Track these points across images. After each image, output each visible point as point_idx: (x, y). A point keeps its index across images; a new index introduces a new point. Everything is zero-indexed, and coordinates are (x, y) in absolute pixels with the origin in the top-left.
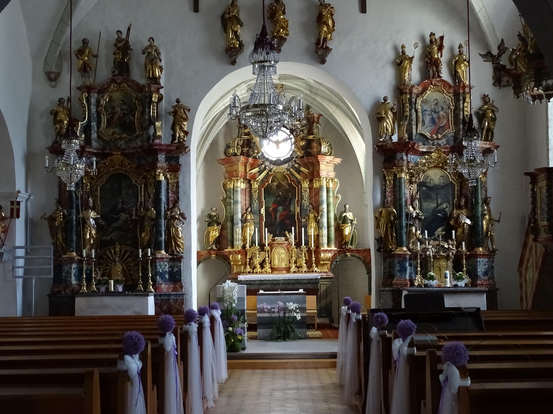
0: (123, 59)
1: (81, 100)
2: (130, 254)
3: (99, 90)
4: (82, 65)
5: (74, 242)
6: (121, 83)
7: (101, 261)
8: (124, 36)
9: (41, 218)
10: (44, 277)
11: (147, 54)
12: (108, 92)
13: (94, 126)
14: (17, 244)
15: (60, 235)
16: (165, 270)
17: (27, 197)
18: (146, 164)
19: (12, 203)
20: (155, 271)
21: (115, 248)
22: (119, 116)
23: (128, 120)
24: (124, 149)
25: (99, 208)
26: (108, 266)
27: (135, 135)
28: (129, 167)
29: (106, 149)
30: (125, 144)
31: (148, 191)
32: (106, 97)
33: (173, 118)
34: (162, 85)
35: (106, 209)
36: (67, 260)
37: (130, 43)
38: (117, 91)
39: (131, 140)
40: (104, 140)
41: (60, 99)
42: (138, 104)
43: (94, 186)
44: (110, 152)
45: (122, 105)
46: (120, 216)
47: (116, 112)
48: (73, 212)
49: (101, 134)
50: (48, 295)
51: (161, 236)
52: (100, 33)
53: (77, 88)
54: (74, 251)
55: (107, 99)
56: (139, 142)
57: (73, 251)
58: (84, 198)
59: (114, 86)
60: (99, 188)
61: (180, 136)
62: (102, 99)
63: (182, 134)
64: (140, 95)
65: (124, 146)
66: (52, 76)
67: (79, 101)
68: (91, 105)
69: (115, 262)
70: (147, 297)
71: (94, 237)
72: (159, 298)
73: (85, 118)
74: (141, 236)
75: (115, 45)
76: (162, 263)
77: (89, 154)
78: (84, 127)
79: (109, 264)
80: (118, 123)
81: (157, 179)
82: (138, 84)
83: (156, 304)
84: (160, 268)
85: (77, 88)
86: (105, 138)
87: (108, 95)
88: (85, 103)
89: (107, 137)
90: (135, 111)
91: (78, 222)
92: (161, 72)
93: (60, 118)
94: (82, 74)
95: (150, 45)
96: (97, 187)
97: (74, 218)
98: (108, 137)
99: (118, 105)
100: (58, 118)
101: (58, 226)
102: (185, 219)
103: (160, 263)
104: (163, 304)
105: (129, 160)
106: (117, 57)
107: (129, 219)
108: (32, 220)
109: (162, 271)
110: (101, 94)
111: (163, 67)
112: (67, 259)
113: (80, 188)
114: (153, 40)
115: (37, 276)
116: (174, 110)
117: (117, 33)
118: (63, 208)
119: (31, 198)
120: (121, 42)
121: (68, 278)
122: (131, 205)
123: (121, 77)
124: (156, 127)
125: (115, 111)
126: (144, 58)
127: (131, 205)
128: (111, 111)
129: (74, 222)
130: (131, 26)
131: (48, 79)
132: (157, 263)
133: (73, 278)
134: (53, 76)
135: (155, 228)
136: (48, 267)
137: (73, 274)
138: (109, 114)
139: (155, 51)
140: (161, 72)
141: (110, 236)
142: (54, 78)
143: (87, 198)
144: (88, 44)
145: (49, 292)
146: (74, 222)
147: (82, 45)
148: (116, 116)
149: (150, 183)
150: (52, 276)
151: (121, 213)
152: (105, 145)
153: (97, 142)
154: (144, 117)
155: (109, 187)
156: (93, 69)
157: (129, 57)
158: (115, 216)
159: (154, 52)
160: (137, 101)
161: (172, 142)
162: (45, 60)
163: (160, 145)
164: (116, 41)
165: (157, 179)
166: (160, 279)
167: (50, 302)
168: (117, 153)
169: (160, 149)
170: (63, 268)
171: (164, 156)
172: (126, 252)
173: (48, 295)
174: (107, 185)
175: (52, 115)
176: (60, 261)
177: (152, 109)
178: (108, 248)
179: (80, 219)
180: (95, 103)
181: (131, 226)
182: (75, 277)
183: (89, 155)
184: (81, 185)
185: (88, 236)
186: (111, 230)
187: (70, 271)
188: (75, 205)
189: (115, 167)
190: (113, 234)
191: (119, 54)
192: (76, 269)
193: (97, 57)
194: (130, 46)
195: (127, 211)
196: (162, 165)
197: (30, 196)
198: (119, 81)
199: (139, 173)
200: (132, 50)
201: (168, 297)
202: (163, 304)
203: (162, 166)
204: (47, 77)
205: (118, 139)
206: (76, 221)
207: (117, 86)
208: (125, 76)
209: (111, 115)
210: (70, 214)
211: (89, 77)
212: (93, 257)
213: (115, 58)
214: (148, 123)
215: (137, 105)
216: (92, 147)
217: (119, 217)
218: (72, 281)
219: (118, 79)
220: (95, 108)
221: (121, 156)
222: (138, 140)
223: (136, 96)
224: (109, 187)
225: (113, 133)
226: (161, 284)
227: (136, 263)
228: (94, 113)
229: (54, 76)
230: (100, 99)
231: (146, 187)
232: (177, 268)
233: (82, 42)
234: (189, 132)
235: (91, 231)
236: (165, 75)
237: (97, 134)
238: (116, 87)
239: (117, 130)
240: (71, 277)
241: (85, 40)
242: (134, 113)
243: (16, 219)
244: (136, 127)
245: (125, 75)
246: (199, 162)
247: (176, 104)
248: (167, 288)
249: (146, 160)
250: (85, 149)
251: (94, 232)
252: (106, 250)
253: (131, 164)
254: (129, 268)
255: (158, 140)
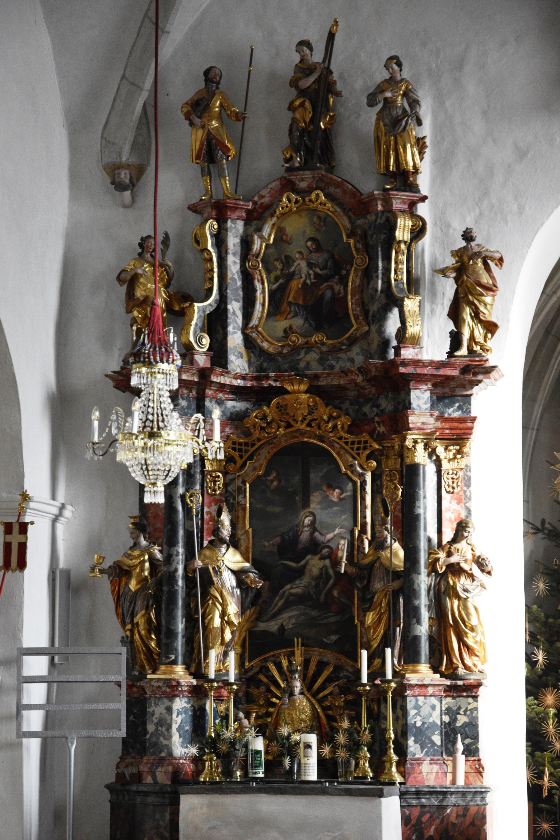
0: (314, 120)
1: (198, 240)
2: (332, 672)
3: (248, 212)
4: (202, 144)
5: (180, 636)
6: (310, 191)
7: (254, 691)
8: (317, 57)
9: (93, 569)
10: (101, 734)
11: (380, 106)
12: (272, 215)
13: (234, 313)
14: (28, 642)
15: (143, 615)
16: (431, 720)
17: (55, 511)
18: (376, 419)
19: (8, 528)
20: (401, 722)
21: (293, 654)
22: (305, 281)
23: (329, 294)
24: (316, 377)
25: (246, 541)
26: (274, 705)
27: (347, 335)
28: (330, 425)
29: (268, 378)
30: (321, 361)
31: (381, 493)
32: (268, 231)
33: (455, 286)
34: (424, 190)
35: (266, 544)
36: (159, 687)
37: (335, 76)
38: (299, 211)
39: (335, 350)
40: (262, 351)
41: (142, 239)
42: (357, 250)
43: (234, 479)
44: (278, 384)
45: (311, 252)
46: (307, 563)
47: (294, 271)
48: (178, 552)
49: (254, 335)
50: (108, 787)
51: (419, 622)
52: (252, 50)
53: (189, 208)
54: (180, 662)
55: (270, 235)
56: (357, 354)
57: (174, 662)
58: (208, 513)
59: (289, 200)
60: (248, 485)
61: (472, 338)
62: (256, 237)
63: (479, 333)
64: (360, 222)
65: (316, 369)
66: (123, 176)
67: (196, 245)
68: (227, 253)
69: (292, 694)
70: (377, 800)
71: (233, 623)
72: (414, 802)
73: (210, 290)
74: (362, 623)
75: (294, 83)
76: (421, 699)
77: (221, 391)
78: (208, 314)
79: (274, 700)
80: (301, 302)
81: (408, 461)
82: (356, 193)
83: (406, 820)
84: (418, 714)
85: (189, 208)
86: (265, 345)
87: (274, 225)
88: (210, 248)
89: (272, 344)
90: (348, 267)
91: (189, 580)
92: (421, 153)
93: (143, 293)
94: (202, 170)
95: (391, 78)
96: (244, 483)
97: (180, 571)
98: (274, 342)
99: (300, 253)
100: (139, 293)
101: (137, 592)
102: (489, 573)
103: (417, 701)
104: (425, 818)
105: (329, 408)
106: (298, 116)
107: (331, 572)
108: (67, 573)
109: (423, 723)
110: (254, 222)
111: (428, 141)
112: (161, 684)
113: (198, 487)
114: (399, 64)
115: (84, 733)
116: (457, 262)
117: (301, 47)
118: (153, 541)
119: (68, 513)
120: (310, 74)
121: (162, 739)
122: (336, 532)
123: (307, 172)
124: (407, 313)
125: (292, 269)
126: (374, 118)
127: (336, 532)
128: (282, 270)
129: (180, 582)
130: (337, 26)
131: (112, 183)
132: (408, 699)
133: (176, 739)
134: (124, 176)
135: (401, 600)
136: (112, 706)
137: (175, 727)
138: (277, 279)
139: (405, 95)
140: (421, 153)
141: (280, 621)
142: (127, 181)
143: (214, 514)
144: (218, 83)
145: (112, 779)
146: (180, 582)
147: (204, 86)
148: (296, 284)
149: (390, 471)
150: (123, 733)
151: (309, 557)
152: (265, 365)
153: (242, 358)
154: (371, 286)
155: (275, 483)
156: (232, 152)
157: (331, 117)
158: (293, 564)
159: (402, 99)
160: (352, 241)
161: (450, 354)
162: (102, 134)
163: (416, 363)
164: (295, 73)
165: (408, 461)
166: (418, 746)
167: (114, 807)
168: (296, 387)
169: (417, 374)
170: (150, 710)
171: (428, 394)
172: (322, 665)
173: (108, 787)
174: (271, 477)
175: (121, 285)
176: (143, 689)
177: (396, 263)
178: (271, 653)
179: (194, 571)
180: (238, 249)
181: (335, 593)
182: (180, 736)
183: (220, 395)
184: (198, 477)
185: (217, 622)
186: (280, 604)
187: (168, 718)
188: (181, 532)
189: (292, 426)
190: (285, 615)
191: (305, 109)
192: (186, 712)
193: (244, 118)
194: (335, 82)
195: (325, 551)
196: (423, 420)
197: (62, 507)
198: (303, 185)
199: (359, 443)
200: (338, 94)
201: (441, 801)
202: (425, 818)
203: (423, 424)
204: (109, 180)
205: (300, 347)
206: (186, 577)
207: (299, 198)
208: (319, 171)
209: (281, 281)
210: (169, 558)
211: (221, 175)
212: (232, 680)
213: (294, 120)
214: (384, 300)
215: (354, 253)
216: (228, 372)
217: (304, 566)
218: (174, 748)
219: (303, 180)
220: (238, 261)
221: (308, 395)
222: (356, 349)
223: (349, 226)
224: (275, 483)
225: (288, 332)
226: (419, 762)
227: (350, 697)
228: (236, 276)
229: (128, 176)
230: (252, 236)
231: (378, 482)
232: (465, 714)
233: (204, 78)
234: (498, 323)
235: (224, 605)
236: (435, 162)
237: (243, 333)
238: (297, 202)
239: (298, 322)
240: (171, 736)
241: (212, 74)
242: (344, 272)
243: (18, 571)
244: (351, 313)
245: (319, 168)
246: (537, 405)
247: (463, 244)
248: (437, 773)
249: (378, 406)
250: (210, 377)
251: (233, 609)
252: (266, 660)
253: (335, 418)
254: (330, 713)
255: (411, 350)
